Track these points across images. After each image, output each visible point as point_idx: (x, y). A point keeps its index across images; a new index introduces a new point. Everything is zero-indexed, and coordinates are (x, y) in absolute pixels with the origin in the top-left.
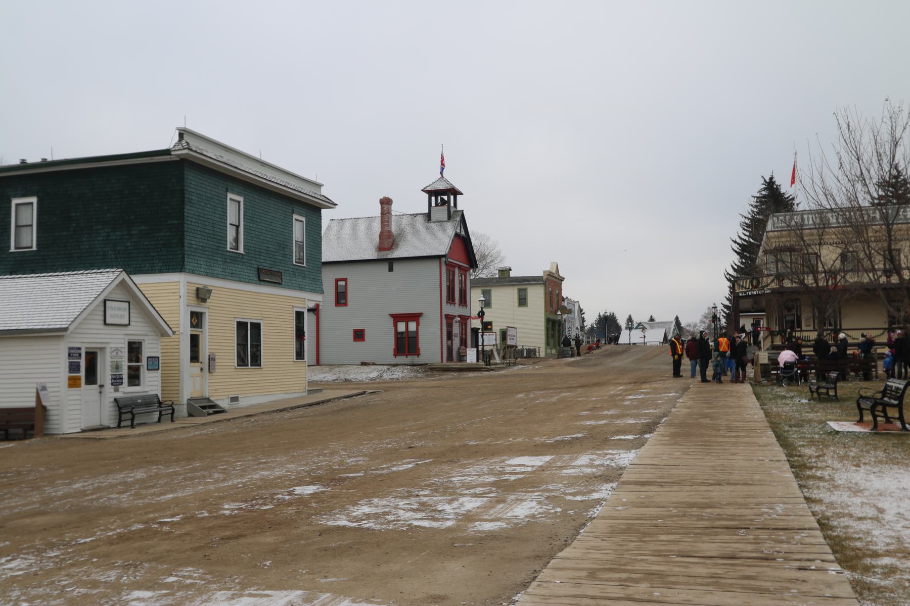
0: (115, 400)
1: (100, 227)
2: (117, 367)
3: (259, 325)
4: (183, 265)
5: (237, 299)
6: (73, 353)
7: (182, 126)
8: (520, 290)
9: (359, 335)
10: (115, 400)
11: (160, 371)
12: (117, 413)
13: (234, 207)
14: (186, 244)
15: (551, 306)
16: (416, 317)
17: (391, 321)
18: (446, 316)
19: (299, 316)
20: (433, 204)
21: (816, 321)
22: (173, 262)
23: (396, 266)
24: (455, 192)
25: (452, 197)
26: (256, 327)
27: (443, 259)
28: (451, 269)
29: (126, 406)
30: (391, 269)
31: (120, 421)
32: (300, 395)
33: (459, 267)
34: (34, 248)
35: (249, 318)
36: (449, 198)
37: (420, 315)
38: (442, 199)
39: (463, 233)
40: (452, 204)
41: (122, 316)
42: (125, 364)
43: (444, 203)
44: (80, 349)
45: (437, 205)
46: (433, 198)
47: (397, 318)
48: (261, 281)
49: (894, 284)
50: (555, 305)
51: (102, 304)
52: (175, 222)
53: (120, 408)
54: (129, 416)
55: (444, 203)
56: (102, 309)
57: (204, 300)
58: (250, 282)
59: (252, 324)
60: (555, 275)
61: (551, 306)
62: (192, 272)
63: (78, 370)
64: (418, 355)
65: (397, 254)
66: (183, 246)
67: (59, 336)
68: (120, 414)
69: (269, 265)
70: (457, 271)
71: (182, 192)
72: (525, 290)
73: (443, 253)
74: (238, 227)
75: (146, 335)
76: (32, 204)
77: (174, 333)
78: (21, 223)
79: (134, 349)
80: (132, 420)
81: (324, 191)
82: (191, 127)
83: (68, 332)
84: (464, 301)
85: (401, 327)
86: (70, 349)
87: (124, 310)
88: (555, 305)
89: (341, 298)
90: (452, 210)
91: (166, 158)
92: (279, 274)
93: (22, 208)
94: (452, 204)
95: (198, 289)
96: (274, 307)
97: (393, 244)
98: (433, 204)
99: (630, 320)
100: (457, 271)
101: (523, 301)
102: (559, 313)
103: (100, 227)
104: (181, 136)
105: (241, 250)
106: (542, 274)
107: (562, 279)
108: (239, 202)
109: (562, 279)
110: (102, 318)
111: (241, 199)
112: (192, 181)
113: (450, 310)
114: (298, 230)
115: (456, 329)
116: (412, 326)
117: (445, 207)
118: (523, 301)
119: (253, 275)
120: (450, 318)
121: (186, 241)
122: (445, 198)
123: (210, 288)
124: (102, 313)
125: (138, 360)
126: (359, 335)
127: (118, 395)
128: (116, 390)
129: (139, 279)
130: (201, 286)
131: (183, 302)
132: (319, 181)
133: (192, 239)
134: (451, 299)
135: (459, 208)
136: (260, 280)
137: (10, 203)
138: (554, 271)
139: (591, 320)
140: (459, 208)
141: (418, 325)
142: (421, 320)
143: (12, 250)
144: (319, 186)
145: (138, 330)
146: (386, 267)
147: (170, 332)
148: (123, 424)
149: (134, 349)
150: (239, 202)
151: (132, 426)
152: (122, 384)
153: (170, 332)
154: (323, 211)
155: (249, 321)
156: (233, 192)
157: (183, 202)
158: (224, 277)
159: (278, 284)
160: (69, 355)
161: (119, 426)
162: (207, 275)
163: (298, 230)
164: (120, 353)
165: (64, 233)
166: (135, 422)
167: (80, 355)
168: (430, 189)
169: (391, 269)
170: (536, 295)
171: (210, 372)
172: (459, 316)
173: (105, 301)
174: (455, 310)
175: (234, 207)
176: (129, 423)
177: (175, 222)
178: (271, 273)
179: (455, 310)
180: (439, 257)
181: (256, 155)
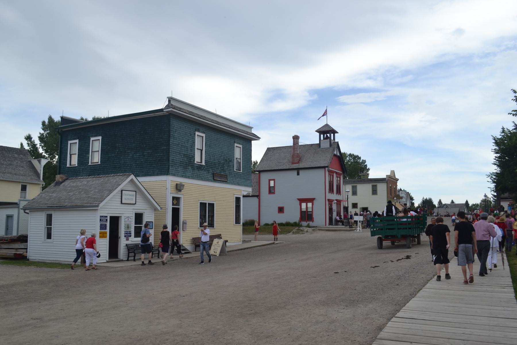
0: (126, 245)
1: (129, 151)
2: (128, 227)
3: (213, 204)
4: (168, 171)
5: (198, 190)
6: (103, 218)
7: (170, 96)
8: (373, 186)
9: (281, 210)
10: (126, 245)
11: (153, 230)
12: (127, 252)
13: (200, 140)
14: (170, 160)
15: (391, 194)
16: (311, 200)
17: (298, 202)
18: (329, 200)
19: (238, 200)
20: (322, 138)
21: (491, 246)
22: (163, 170)
23: (301, 172)
24: (334, 132)
25: (332, 135)
26: (212, 206)
27: (327, 168)
28: (331, 174)
29: (132, 249)
30: (298, 174)
31: (129, 257)
32: (237, 243)
33: (336, 173)
34: (99, 163)
35: (207, 200)
36: (330, 136)
37: (314, 199)
38: (327, 136)
39: (338, 154)
40: (332, 138)
41: (132, 199)
42: (133, 225)
43: (327, 138)
44: (107, 217)
45: (324, 139)
46: (322, 136)
47: (301, 201)
48: (215, 180)
49: (15, 237)
50: (393, 195)
51: (120, 193)
52: (165, 148)
53: (128, 250)
54: (133, 254)
55: (327, 138)
56: (120, 195)
57: (180, 191)
58: (208, 180)
59: (209, 204)
60: (393, 178)
61: (391, 194)
62: (174, 175)
63: (106, 229)
64: (313, 221)
65: (301, 165)
66: (169, 161)
67: (95, 210)
68: (129, 253)
69: (218, 170)
70: (335, 175)
71: (169, 131)
72: (376, 186)
73: (326, 165)
74: (202, 150)
75: (146, 209)
76: (99, 140)
77: (161, 208)
78: (93, 150)
79: (139, 217)
80: (134, 256)
81: (254, 131)
82: (175, 96)
83: (99, 208)
84: (339, 192)
85: (304, 205)
86: (101, 217)
87: (133, 195)
88: (393, 195)
89: (272, 190)
90: (332, 142)
91: (161, 113)
92: (226, 176)
93: (94, 142)
94: (332, 138)
95: (177, 184)
96: (223, 195)
97: (300, 160)
98: (322, 138)
99: (440, 202)
100: (335, 175)
101: (374, 192)
102: (395, 198)
103: (129, 151)
104: (169, 101)
105: (203, 163)
106: (385, 177)
107: (397, 180)
108: (203, 137)
109: (397, 180)
110: (120, 200)
111: (204, 135)
112: (175, 124)
113: (330, 196)
114: (238, 153)
115: (334, 207)
116: (310, 205)
117: (328, 140)
118: (374, 192)
119: (210, 176)
120: (330, 201)
121: (171, 158)
122: (329, 135)
123: (183, 184)
124: (120, 197)
125: (141, 223)
126: (281, 210)
127: (128, 242)
128: (127, 240)
129: (141, 179)
130: (178, 183)
131: (169, 191)
132: (251, 126)
133: (175, 157)
134: (331, 190)
135: (336, 141)
136: (214, 180)
137: (90, 140)
138: (392, 175)
139: (417, 203)
140: (336, 141)
141: (313, 205)
142: (314, 201)
143: (90, 164)
144: (251, 128)
145: (141, 207)
146: (295, 172)
147: (159, 208)
148: (130, 258)
149: (139, 217)
150: (203, 137)
151: (134, 260)
152: (131, 236)
153: (159, 208)
154: (253, 142)
155: (207, 202)
156: (199, 131)
157: (169, 137)
158: (193, 178)
159: (226, 182)
160: (100, 220)
161: (128, 260)
162: (182, 176)
163: (238, 153)
164: (130, 219)
165: (113, 155)
166: (136, 258)
167: (107, 220)
168: (321, 130)
169: (298, 174)
170: (382, 188)
171: (183, 230)
172: (336, 200)
173: (122, 191)
174: (334, 197)
175: (200, 140)
176: (133, 258)
177: (165, 148)
178: (221, 176)
179: (334, 197)
180: (324, 167)
181: (214, 112)
